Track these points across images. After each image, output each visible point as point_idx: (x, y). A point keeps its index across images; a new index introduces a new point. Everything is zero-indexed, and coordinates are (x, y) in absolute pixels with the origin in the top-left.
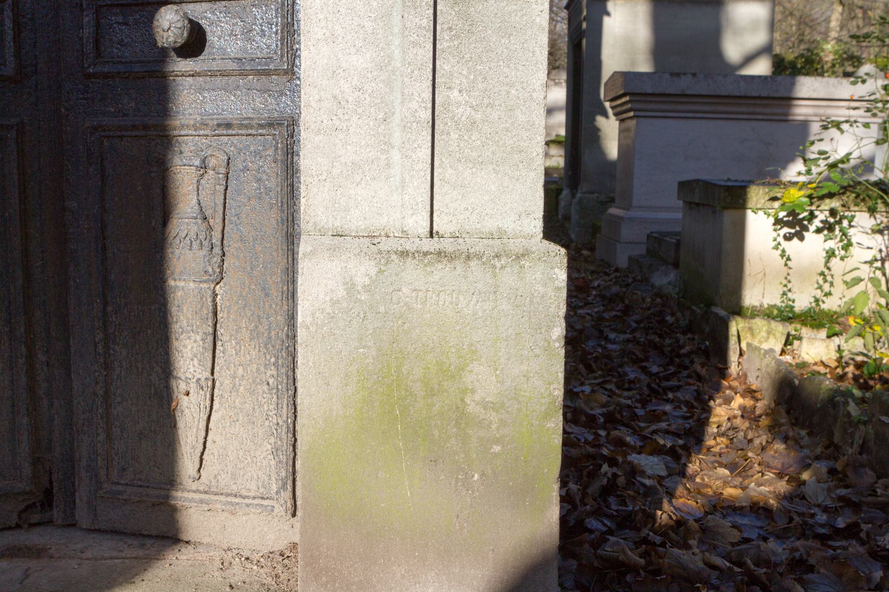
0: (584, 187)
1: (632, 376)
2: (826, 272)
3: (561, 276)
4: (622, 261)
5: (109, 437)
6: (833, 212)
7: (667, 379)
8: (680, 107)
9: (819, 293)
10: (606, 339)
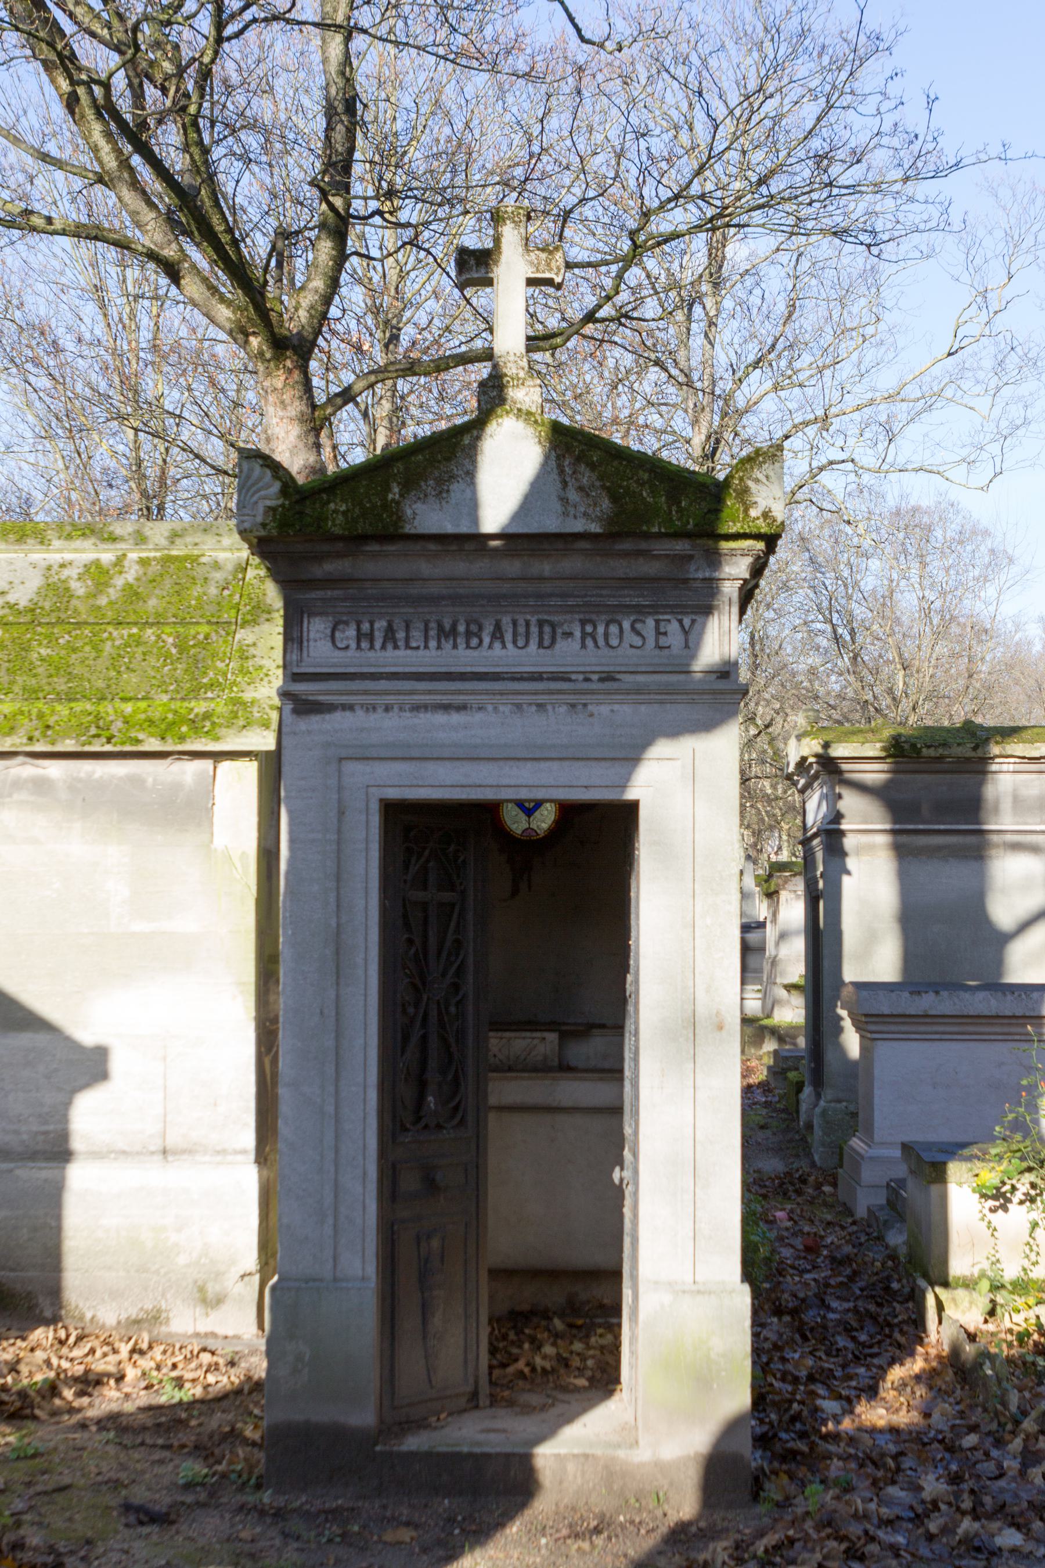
0: (828, 1093)
2: (1032, 1242)
3: (748, 1300)
4: (861, 1212)
6: (1033, 1186)
7: (871, 1347)
8: (922, 1028)
9: (1026, 1264)
10: (828, 1308)
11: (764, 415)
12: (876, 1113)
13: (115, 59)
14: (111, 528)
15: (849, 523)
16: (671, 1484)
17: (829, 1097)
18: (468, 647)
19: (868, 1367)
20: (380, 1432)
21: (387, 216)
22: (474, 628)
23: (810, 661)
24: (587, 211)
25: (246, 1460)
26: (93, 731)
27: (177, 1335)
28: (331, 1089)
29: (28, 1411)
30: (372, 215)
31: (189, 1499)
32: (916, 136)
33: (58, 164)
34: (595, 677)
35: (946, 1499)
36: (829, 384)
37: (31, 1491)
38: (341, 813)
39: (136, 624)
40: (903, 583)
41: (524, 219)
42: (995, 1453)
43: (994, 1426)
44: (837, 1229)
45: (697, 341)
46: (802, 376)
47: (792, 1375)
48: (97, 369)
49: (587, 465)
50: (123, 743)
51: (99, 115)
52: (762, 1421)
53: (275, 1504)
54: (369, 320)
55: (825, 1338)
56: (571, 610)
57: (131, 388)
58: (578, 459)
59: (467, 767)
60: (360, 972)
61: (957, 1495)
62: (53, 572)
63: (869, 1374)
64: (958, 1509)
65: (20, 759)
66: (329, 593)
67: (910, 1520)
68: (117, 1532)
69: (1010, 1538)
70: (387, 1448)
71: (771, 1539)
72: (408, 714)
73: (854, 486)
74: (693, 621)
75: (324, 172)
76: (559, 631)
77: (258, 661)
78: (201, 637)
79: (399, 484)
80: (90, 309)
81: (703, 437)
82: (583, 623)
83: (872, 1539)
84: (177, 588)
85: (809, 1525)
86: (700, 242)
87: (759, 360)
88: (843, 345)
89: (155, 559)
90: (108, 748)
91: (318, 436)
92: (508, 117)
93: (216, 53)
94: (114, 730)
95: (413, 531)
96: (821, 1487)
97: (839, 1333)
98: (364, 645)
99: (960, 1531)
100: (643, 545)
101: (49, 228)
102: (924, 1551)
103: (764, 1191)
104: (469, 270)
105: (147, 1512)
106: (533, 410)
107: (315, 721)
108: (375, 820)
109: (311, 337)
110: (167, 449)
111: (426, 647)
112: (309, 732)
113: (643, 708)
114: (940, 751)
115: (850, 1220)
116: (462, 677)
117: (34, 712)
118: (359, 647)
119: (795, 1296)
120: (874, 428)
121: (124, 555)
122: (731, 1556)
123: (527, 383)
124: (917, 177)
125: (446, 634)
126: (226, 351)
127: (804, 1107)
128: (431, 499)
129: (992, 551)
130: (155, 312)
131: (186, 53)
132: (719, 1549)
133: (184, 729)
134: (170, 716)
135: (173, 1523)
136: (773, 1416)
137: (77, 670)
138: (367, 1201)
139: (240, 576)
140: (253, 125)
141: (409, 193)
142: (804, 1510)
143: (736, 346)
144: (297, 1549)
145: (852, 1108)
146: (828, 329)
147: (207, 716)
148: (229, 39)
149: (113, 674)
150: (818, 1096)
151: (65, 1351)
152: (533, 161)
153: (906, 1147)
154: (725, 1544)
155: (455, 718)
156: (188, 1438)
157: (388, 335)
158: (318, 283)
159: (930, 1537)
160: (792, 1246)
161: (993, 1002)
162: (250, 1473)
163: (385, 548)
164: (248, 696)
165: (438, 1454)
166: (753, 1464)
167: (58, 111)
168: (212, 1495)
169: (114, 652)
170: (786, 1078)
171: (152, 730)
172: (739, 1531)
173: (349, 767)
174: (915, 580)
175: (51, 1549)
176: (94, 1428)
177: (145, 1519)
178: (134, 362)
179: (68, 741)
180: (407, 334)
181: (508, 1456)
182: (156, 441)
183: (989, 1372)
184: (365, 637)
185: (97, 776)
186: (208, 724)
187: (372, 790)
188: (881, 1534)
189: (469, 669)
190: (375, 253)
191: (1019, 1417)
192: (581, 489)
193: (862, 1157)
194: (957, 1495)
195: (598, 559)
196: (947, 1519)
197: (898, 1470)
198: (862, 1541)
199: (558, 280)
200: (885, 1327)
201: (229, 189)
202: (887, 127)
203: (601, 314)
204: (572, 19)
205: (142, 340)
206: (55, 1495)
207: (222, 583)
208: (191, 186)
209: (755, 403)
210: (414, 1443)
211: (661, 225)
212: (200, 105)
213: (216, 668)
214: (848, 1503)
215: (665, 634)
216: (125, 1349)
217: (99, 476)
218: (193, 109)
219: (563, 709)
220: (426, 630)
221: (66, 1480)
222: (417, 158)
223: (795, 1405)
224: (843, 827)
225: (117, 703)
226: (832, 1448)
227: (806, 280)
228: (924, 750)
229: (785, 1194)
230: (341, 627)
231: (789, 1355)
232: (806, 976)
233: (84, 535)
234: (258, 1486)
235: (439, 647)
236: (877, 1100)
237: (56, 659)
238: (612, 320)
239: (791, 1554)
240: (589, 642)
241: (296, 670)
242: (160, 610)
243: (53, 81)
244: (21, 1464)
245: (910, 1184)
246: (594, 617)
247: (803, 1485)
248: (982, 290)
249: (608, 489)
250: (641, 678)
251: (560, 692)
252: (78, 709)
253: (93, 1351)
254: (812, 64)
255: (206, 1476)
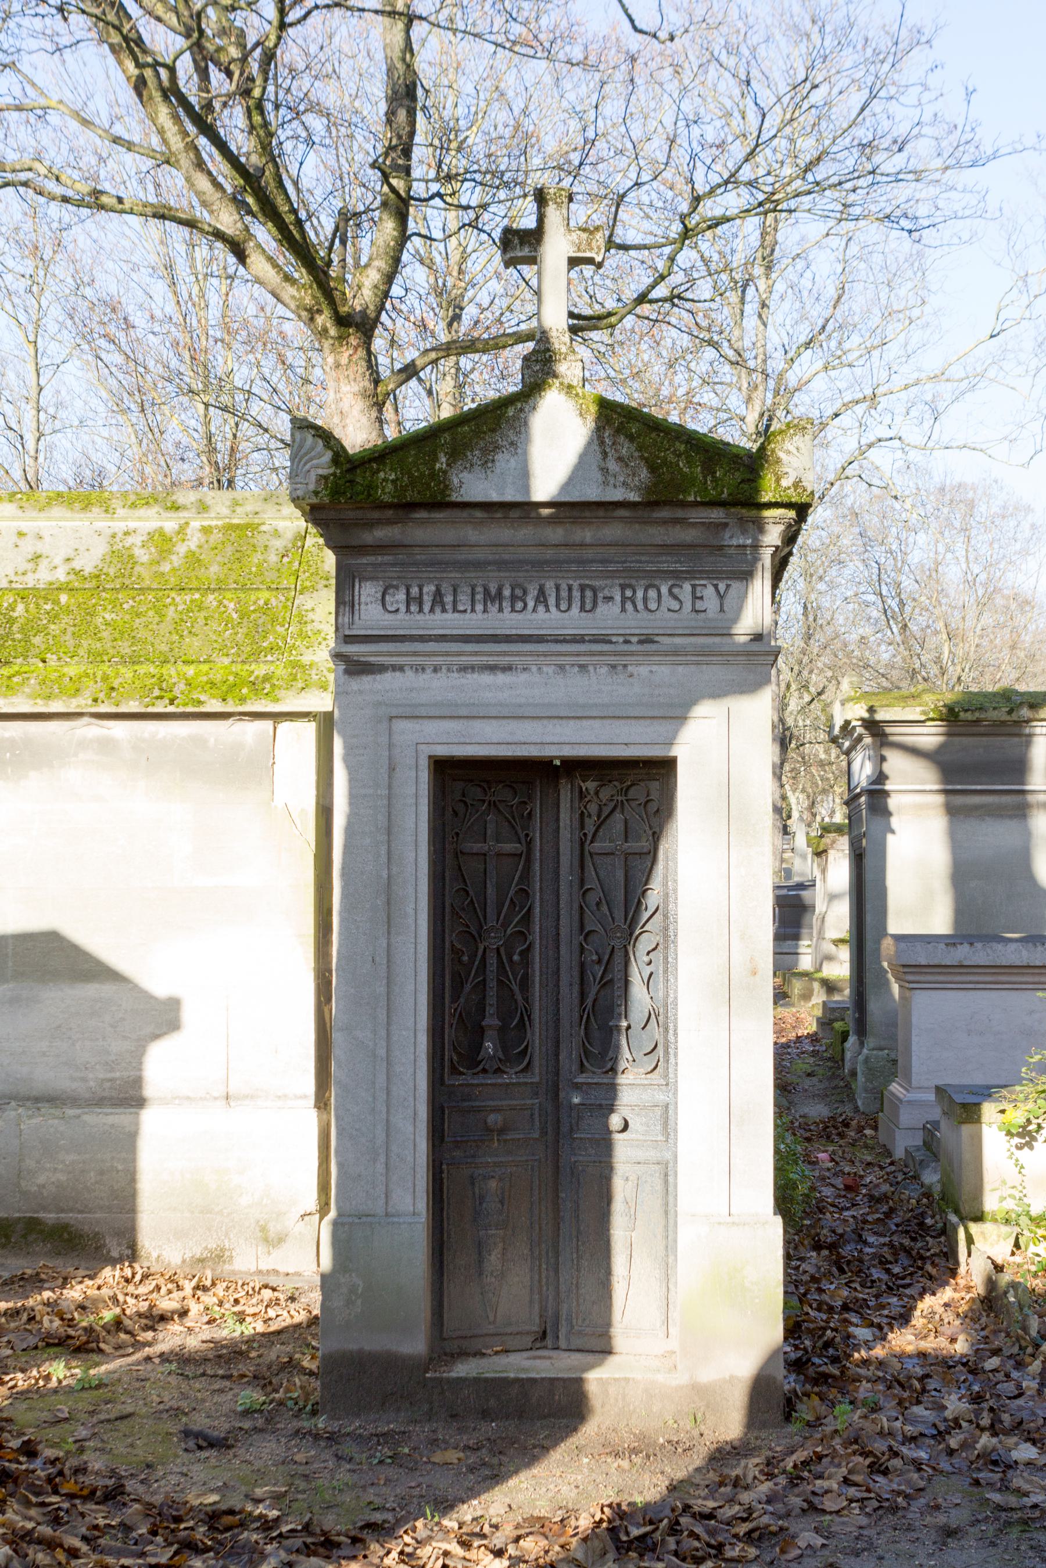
0: (871, 1042)
1: (875, 1277)
3: (781, 1231)
5: (578, 1305)
7: (903, 1278)
11: (814, 394)
12: (914, 1058)
13: (181, 42)
14: (174, 498)
15: (896, 498)
16: (707, 1406)
17: (871, 1045)
18: (513, 610)
19: (900, 1297)
20: (431, 1359)
21: (448, 199)
22: (519, 592)
23: (861, 631)
24: (643, 195)
25: (301, 1387)
26: (157, 692)
27: (241, 1272)
28: (383, 1033)
29: (94, 1345)
30: (432, 197)
31: (247, 1425)
32: (955, 127)
33: (129, 146)
34: (634, 639)
35: (967, 1417)
36: (877, 364)
37: (95, 1420)
38: (392, 769)
39: (198, 589)
40: (949, 556)
41: (566, 200)
42: (1015, 1374)
43: (1015, 1350)
44: (876, 1169)
45: (751, 322)
46: (851, 357)
47: (827, 1304)
48: (168, 344)
49: (626, 436)
50: (185, 705)
51: (166, 97)
52: (796, 1348)
53: (329, 1429)
54: (432, 299)
55: (860, 1271)
56: (611, 575)
57: (199, 361)
58: (618, 431)
59: (512, 725)
60: (411, 921)
61: (978, 1413)
62: (118, 539)
63: (901, 1303)
64: (978, 1426)
65: (86, 720)
66: (380, 558)
67: (933, 1437)
68: (177, 1456)
69: (1026, 1452)
70: (438, 1375)
71: (800, 1456)
72: (456, 675)
73: (902, 462)
74: (728, 586)
75: (386, 154)
76: (600, 595)
77: (317, 626)
78: (261, 602)
79: (446, 454)
80: (160, 288)
81: (756, 415)
82: (623, 587)
83: (896, 1454)
84: (238, 555)
85: (837, 1442)
86: (752, 225)
87: (811, 341)
88: (890, 327)
89: (216, 527)
90: (171, 709)
91: (380, 411)
92: (565, 104)
93: (279, 38)
94: (176, 692)
95: (459, 499)
96: (849, 1408)
97: (874, 1266)
98: (414, 608)
99: (978, 1446)
100: (680, 513)
101: (120, 206)
102: (944, 1465)
103: (808, 1134)
104: (514, 249)
105: (205, 1438)
106: (575, 383)
107: (366, 682)
108: (425, 776)
109: (373, 315)
110: (237, 425)
111: (473, 610)
112: (361, 692)
113: (680, 668)
114: (977, 714)
115: (888, 1161)
116: (508, 639)
117: (99, 674)
118: (408, 610)
119: (834, 1232)
120: (921, 406)
121: (187, 523)
122: (761, 1471)
123: (569, 358)
124: (959, 165)
125: (493, 597)
126: (295, 329)
127: (848, 1055)
128: (477, 468)
129: (1033, 526)
130: (224, 291)
131: (251, 40)
132: (750, 1466)
133: (245, 691)
134: (231, 678)
135: (229, 1447)
136: (808, 1343)
137: (142, 634)
138: (418, 1139)
139: (299, 544)
140: (315, 108)
141: (468, 176)
142: (833, 1428)
143: (788, 327)
144: (349, 1470)
145: (893, 1056)
146: (876, 311)
147: (266, 678)
148: (291, 25)
149: (175, 637)
150: (862, 1044)
151: (131, 1288)
152: (588, 147)
153: (939, 1090)
154: (757, 1460)
155: (501, 678)
156: (246, 1368)
157: (451, 313)
158: (381, 264)
159: (951, 1452)
160: (833, 1186)
161: (1024, 953)
162: (306, 1400)
163: (433, 515)
164: (306, 659)
165: (486, 1380)
166: (787, 1387)
167: (128, 95)
168: (268, 1421)
169: (177, 617)
170: (832, 1029)
171: (214, 691)
172: (770, 1449)
173: (400, 725)
174: (961, 553)
175: (113, 1473)
176: (157, 1361)
177: (205, 1444)
178: (203, 339)
179: (131, 703)
180: (470, 312)
181: (552, 1380)
182: (227, 415)
183: (1012, 1299)
184: (414, 601)
185: (160, 736)
186: (268, 686)
187: (421, 747)
188: (904, 1450)
189: (514, 632)
190: (437, 234)
191: (1039, 1341)
192: (620, 459)
193: (900, 1100)
194: (978, 1413)
195: (637, 526)
196: (967, 1435)
197: (924, 1390)
198: (886, 1457)
199: (598, 259)
200: (919, 1259)
201: (294, 171)
202: (927, 117)
203: (655, 294)
204: (626, 11)
205: (210, 317)
206: (117, 1423)
207: (282, 551)
208: (257, 168)
209: (806, 383)
210: (463, 1369)
211: (710, 208)
212: (264, 89)
213: (276, 632)
214: (873, 1421)
215: (701, 598)
216: (188, 1286)
217: (171, 450)
218: (257, 93)
219: (604, 670)
220: (473, 595)
221: (129, 1409)
222: (475, 140)
223: (829, 1332)
224: (887, 787)
225: (180, 665)
226: (862, 1371)
227: (855, 264)
228: (962, 714)
229: (828, 1137)
230: (391, 591)
231: (825, 1285)
232: (850, 931)
233: (147, 503)
234: (314, 1413)
235: (485, 611)
236: (914, 1048)
237: (121, 623)
238: (664, 300)
239: (819, 1468)
240: (629, 606)
241: (347, 633)
242: (222, 577)
243: (120, 63)
244: (85, 1395)
245: (943, 1125)
246: (633, 582)
247: (833, 1405)
248: (1023, 274)
249: (646, 460)
250: (678, 640)
251: (601, 653)
252: (142, 672)
253: (158, 1288)
254: (856, 56)
255: (264, 1403)
